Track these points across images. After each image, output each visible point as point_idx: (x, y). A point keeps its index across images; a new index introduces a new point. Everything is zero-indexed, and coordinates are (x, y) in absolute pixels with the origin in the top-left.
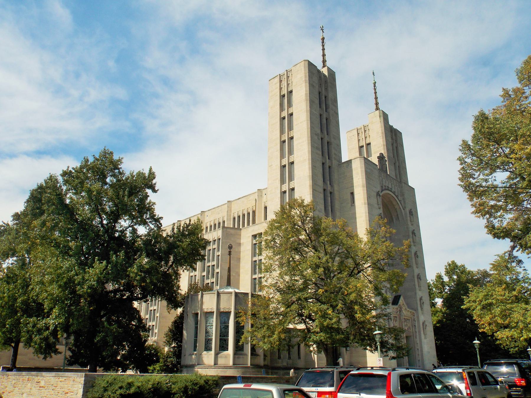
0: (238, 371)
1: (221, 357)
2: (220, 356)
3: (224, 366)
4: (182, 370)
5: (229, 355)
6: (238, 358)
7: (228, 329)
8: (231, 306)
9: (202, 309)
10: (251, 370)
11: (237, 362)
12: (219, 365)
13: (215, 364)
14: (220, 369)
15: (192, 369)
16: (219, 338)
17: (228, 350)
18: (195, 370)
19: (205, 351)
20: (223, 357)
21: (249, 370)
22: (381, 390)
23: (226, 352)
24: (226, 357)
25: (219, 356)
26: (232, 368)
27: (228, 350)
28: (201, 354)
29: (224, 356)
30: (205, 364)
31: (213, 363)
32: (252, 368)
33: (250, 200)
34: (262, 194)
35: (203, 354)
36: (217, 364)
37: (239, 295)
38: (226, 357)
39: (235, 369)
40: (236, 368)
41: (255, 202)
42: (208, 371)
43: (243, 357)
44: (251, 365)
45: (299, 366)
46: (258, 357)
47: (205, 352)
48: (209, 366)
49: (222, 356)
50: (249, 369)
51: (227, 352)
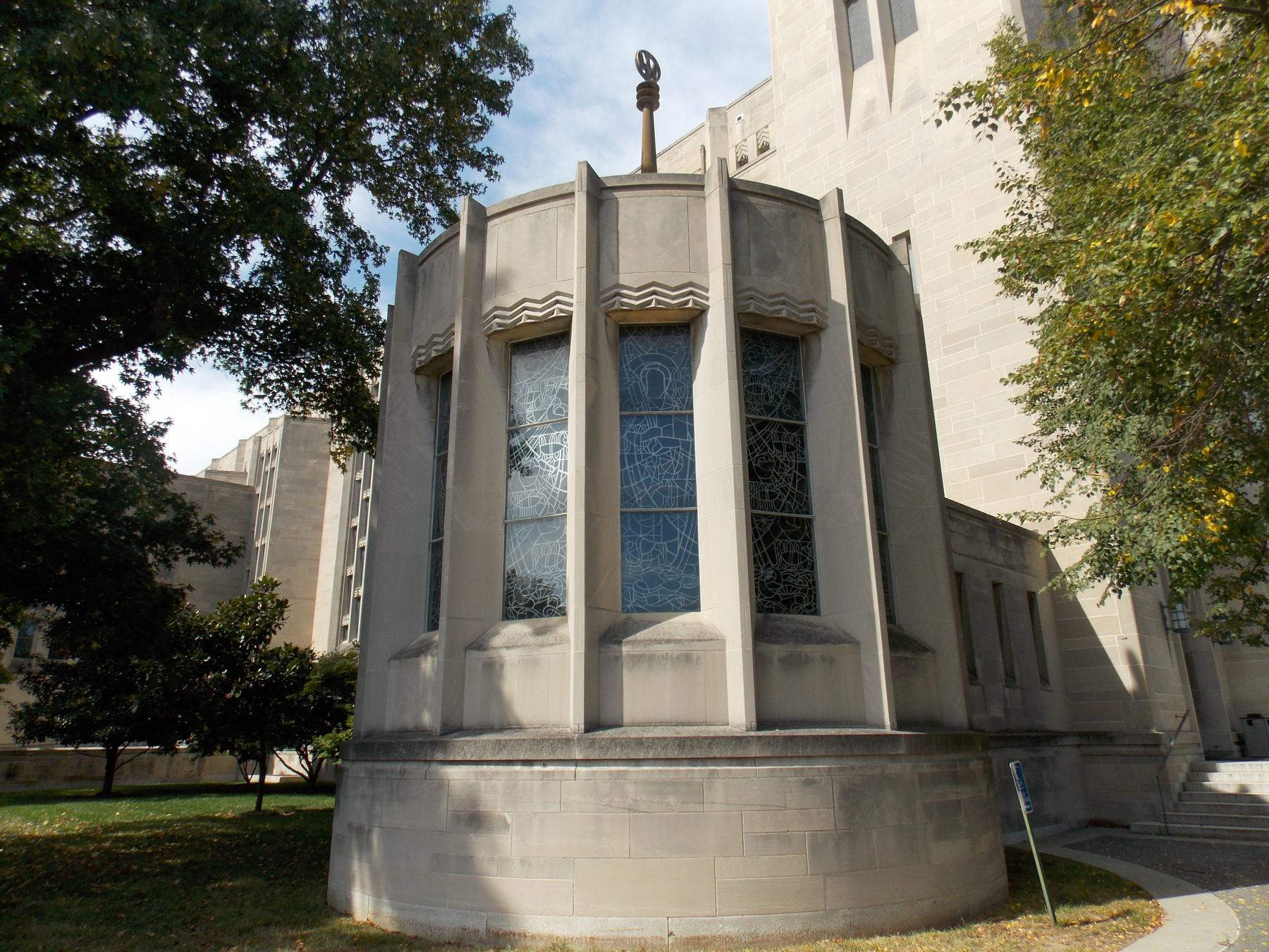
0: (809, 782)
1: (648, 660)
2: (638, 650)
3: (682, 742)
4: (447, 742)
5: (715, 641)
6: (792, 663)
7: (689, 447)
8: (706, 273)
9: (474, 316)
10: (902, 768)
11: (783, 705)
12: (634, 733)
13: (593, 724)
14: (638, 762)
15: (398, 766)
16: (618, 510)
17: (695, 607)
18: (442, 785)
19: (508, 616)
20: (665, 657)
21: (893, 768)
22: (1210, 789)
23: (682, 623)
24: (687, 658)
25: (625, 649)
26: (754, 751)
27: (695, 607)
28: (479, 645)
29: (664, 648)
30: (520, 728)
31: (572, 716)
32: (919, 748)
33: (681, 159)
34: (726, 120)
35: (497, 641)
36: (607, 716)
37: (753, 200)
38: (687, 658)
39: (780, 759)
40: (787, 751)
41: (699, 156)
42: (537, 785)
43: (829, 661)
44: (900, 723)
45: (1176, 727)
46: (927, 656)
47: (518, 629)
48: (539, 742)
49: (656, 648)
50: (894, 758)
51: (689, 617)
